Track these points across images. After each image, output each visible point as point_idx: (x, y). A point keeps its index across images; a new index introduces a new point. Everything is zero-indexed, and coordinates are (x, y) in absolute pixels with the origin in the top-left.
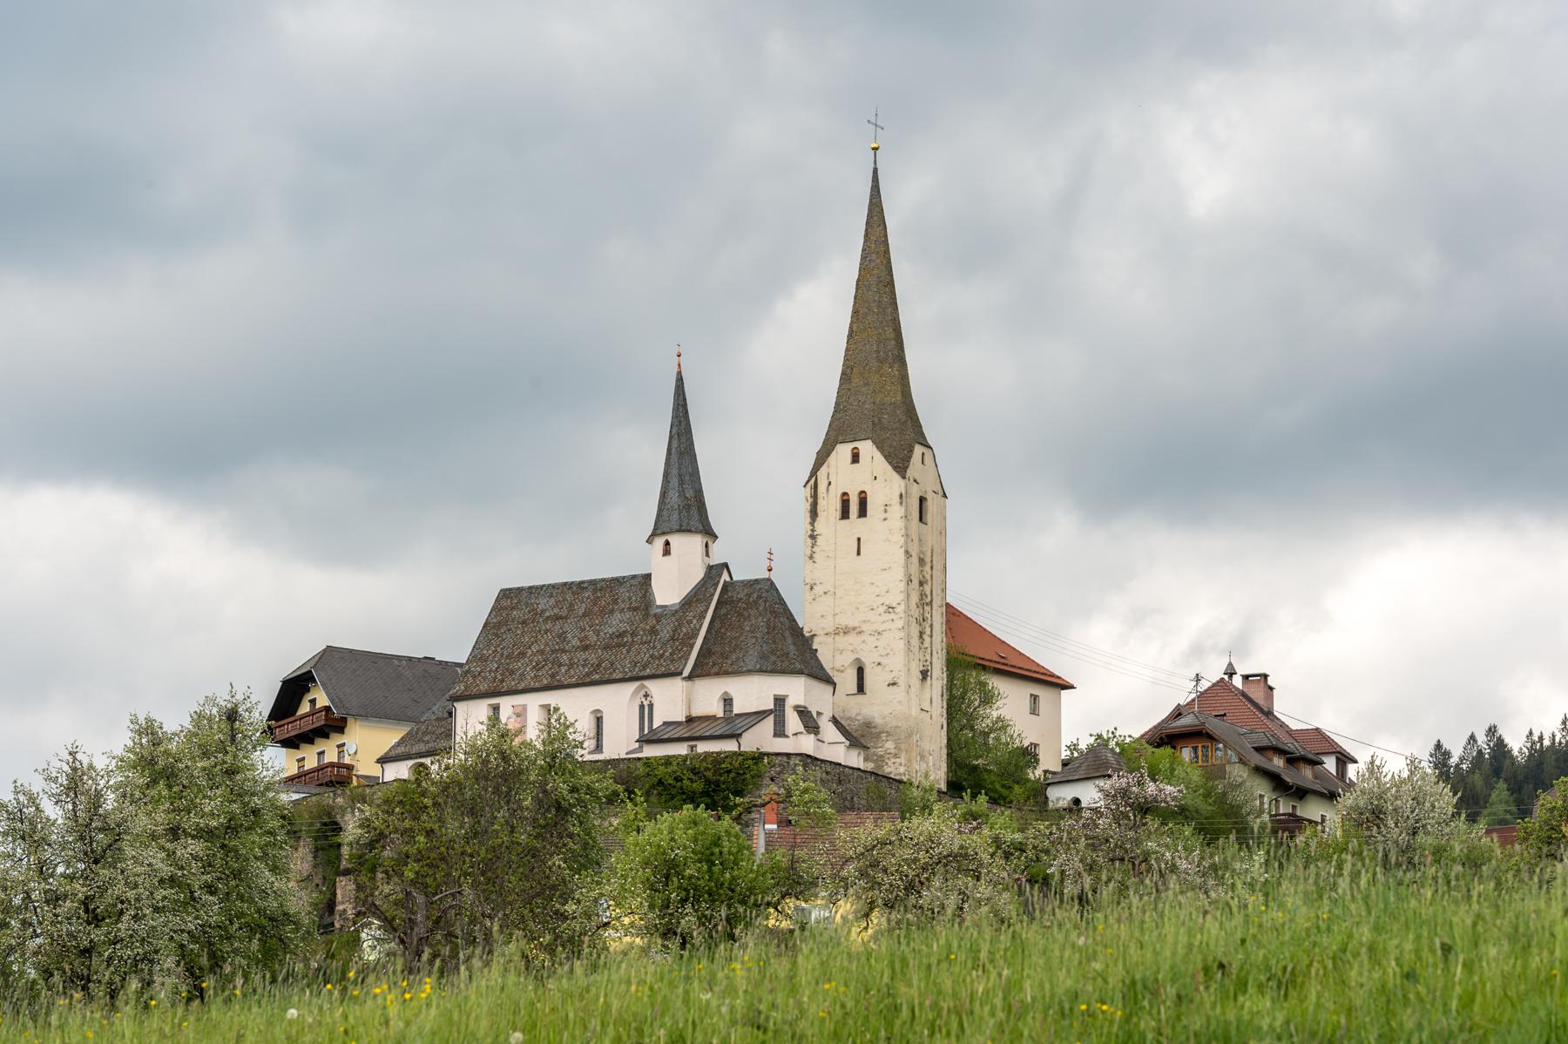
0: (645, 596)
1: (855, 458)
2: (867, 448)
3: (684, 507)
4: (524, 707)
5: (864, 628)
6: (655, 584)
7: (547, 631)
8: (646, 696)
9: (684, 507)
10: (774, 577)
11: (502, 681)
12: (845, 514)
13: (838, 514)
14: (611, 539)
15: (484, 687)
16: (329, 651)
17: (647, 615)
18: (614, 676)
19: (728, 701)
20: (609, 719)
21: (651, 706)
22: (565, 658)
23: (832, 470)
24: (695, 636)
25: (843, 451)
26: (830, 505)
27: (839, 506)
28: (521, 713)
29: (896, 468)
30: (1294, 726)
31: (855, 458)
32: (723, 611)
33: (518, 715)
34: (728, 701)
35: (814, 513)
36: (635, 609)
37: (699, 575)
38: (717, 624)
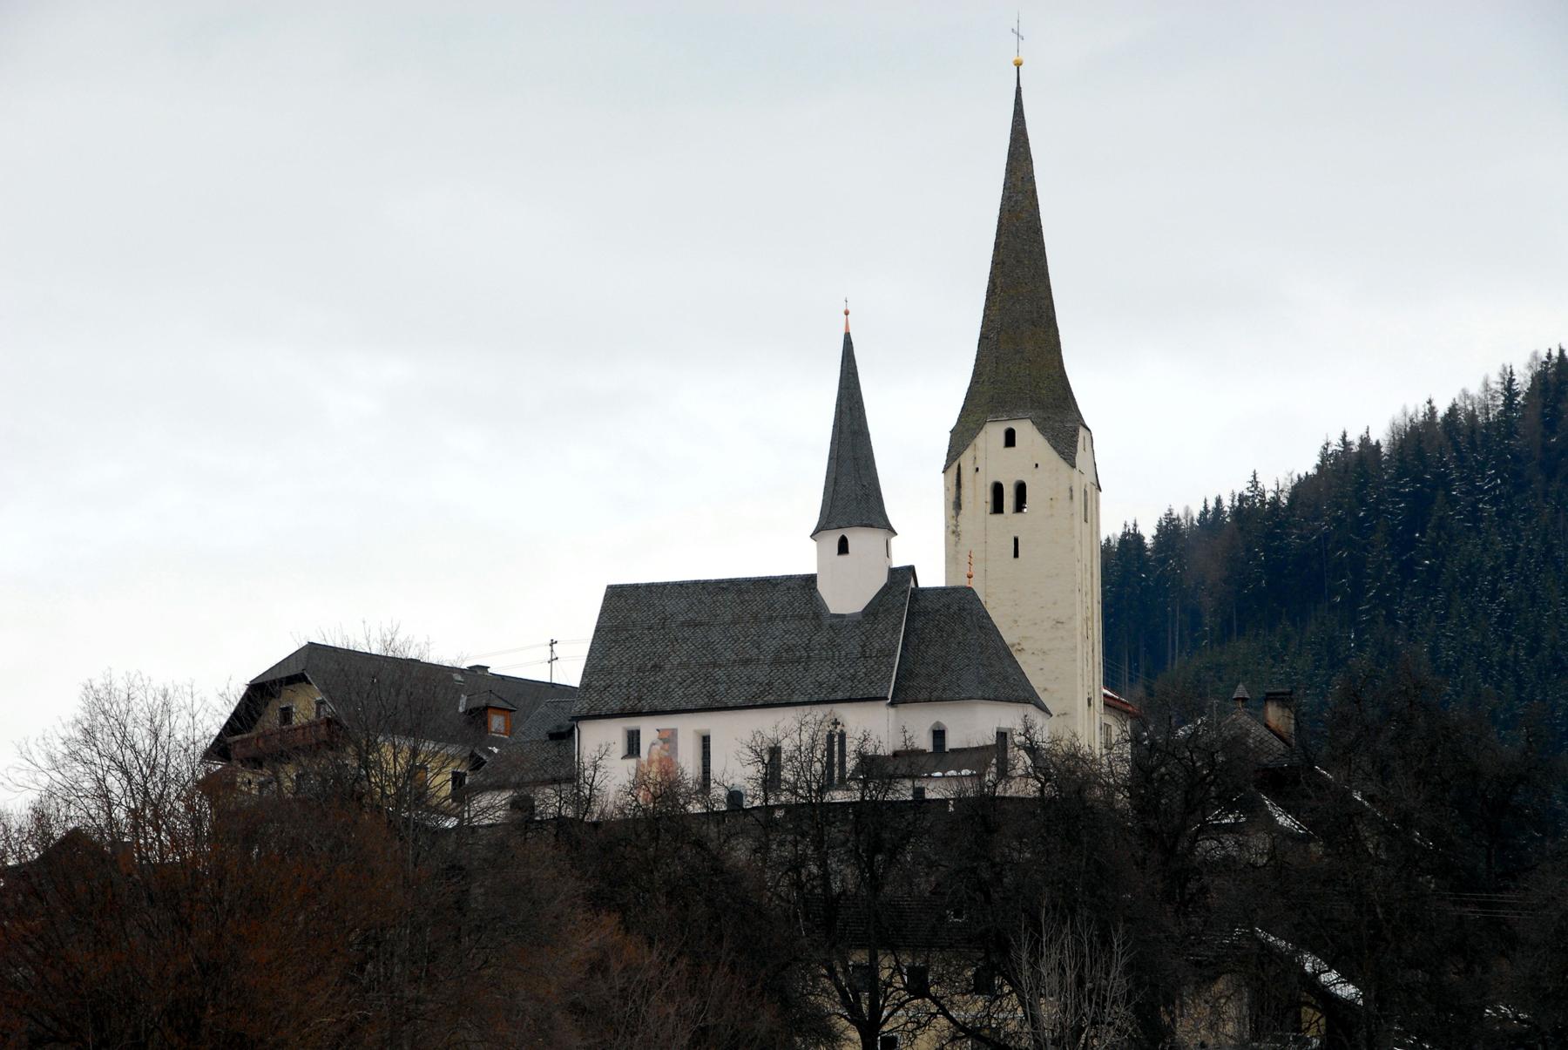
0: (811, 596)
1: (1010, 438)
2: (1026, 431)
3: (852, 496)
4: (674, 732)
5: (1025, 645)
6: (823, 588)
7: (685, 640)
8: (836, 723)
9: (852, 496)
10: (977, 586)
11: (640, 699)
12: (998, 507)
13: (989, 507)
14: (764, 530)
15: (615, 706)
16: (313, 652)
17: (818, 627)
18: (795, 699)
19: (939, 735)
20: (728, 750)
21: (842, 736)
22: (720, 673)
23: (980, 454)
24: (892, 654)
25: (993, 433)
26: (977, 496)
27: (989, 497)
28: (669, 739)
29: (1060, 453)
30: (464, 666)
31: (1010, 438)
32: (918, 624)
33: (665, 741)
34: (939, 735)
35: (957, 505)
36: (802, 618)
37: (882, 580)
38: (914, 640)
